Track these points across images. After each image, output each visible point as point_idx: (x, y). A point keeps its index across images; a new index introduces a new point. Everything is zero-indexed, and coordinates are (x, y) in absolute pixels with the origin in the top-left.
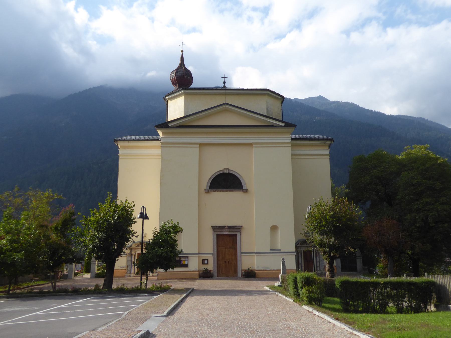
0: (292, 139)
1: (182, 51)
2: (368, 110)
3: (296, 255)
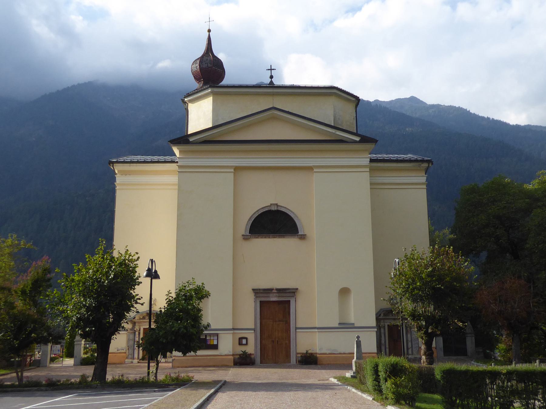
0: (372, 161)
2: (483, 118)
3: (376, 331)
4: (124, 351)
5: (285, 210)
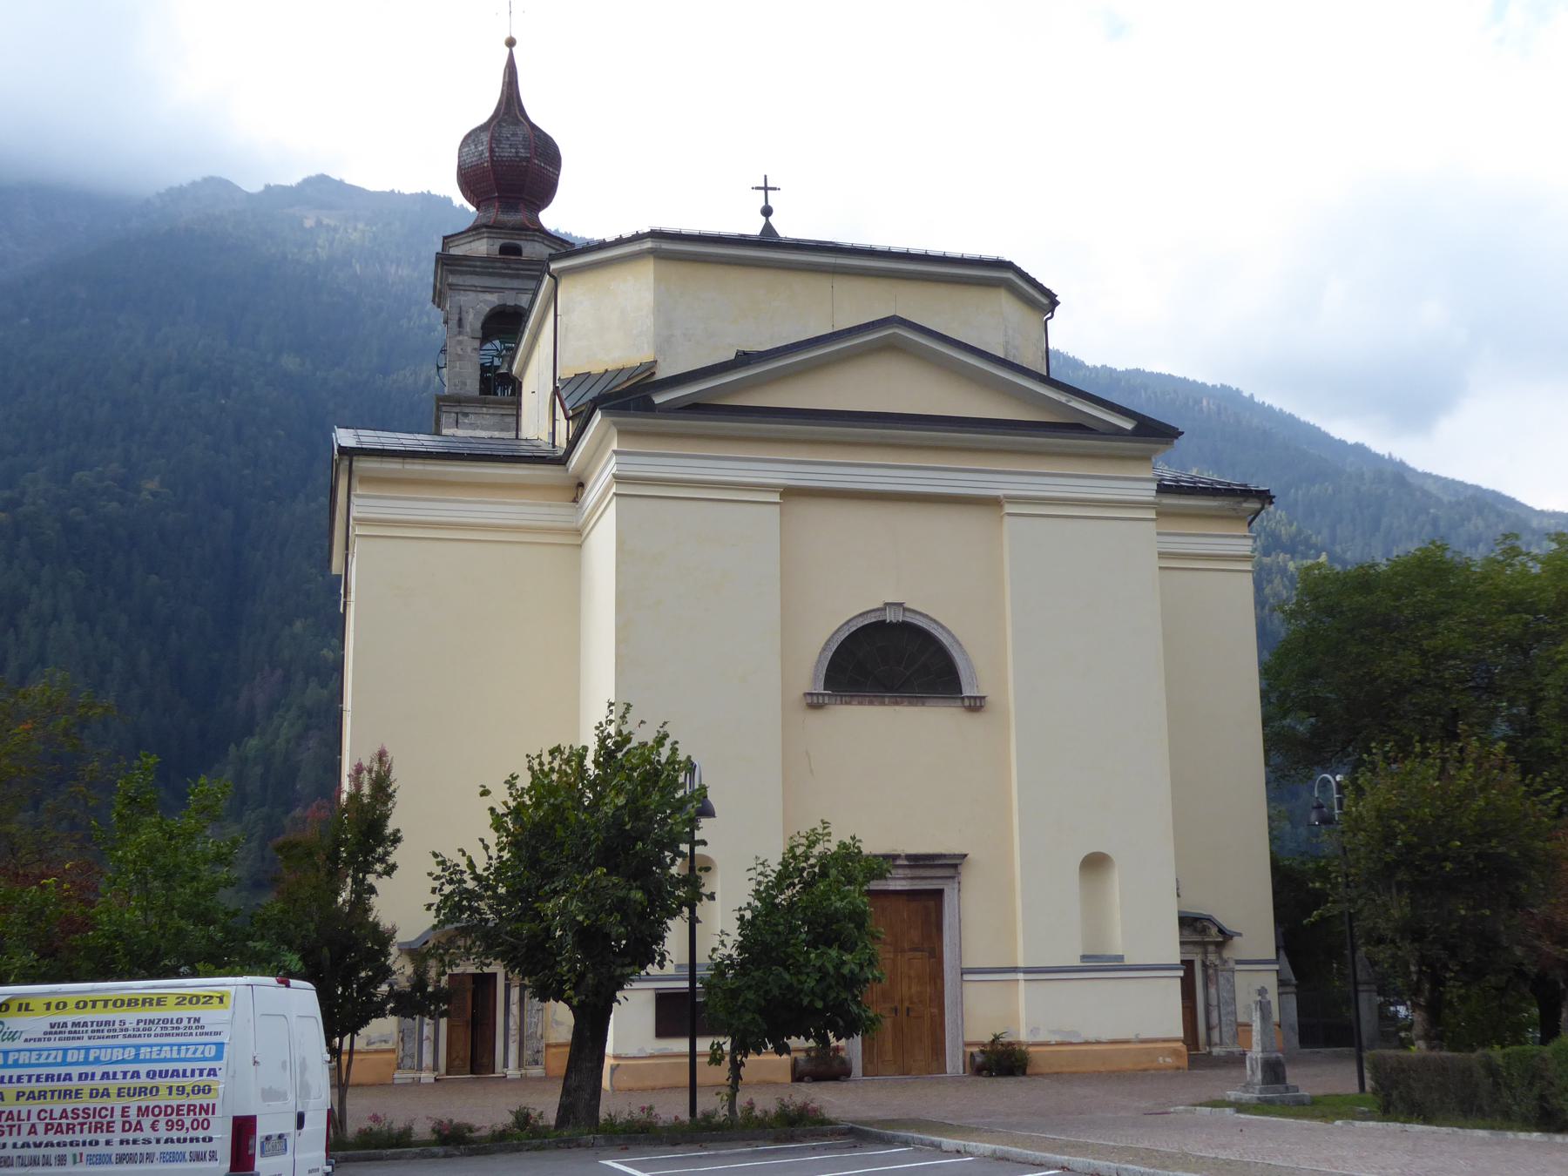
0: (1163, 489)
1: (511, 43)
3: (1182, 978)
5: (875, 617)
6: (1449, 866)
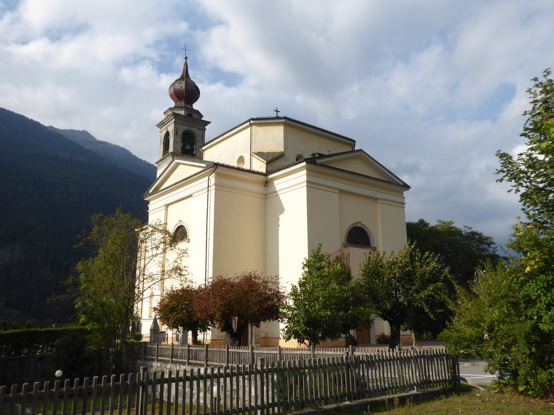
1: (186, 58)
2: (141, 160)
4: (223, 338)
6: (181, 293)
